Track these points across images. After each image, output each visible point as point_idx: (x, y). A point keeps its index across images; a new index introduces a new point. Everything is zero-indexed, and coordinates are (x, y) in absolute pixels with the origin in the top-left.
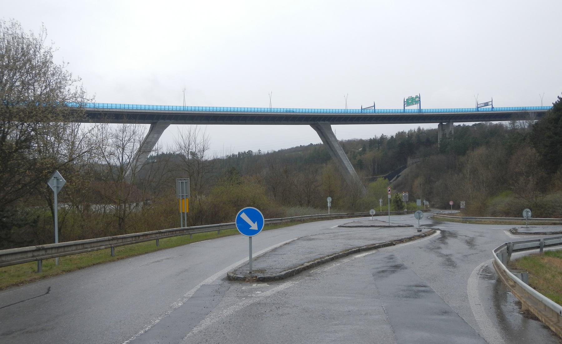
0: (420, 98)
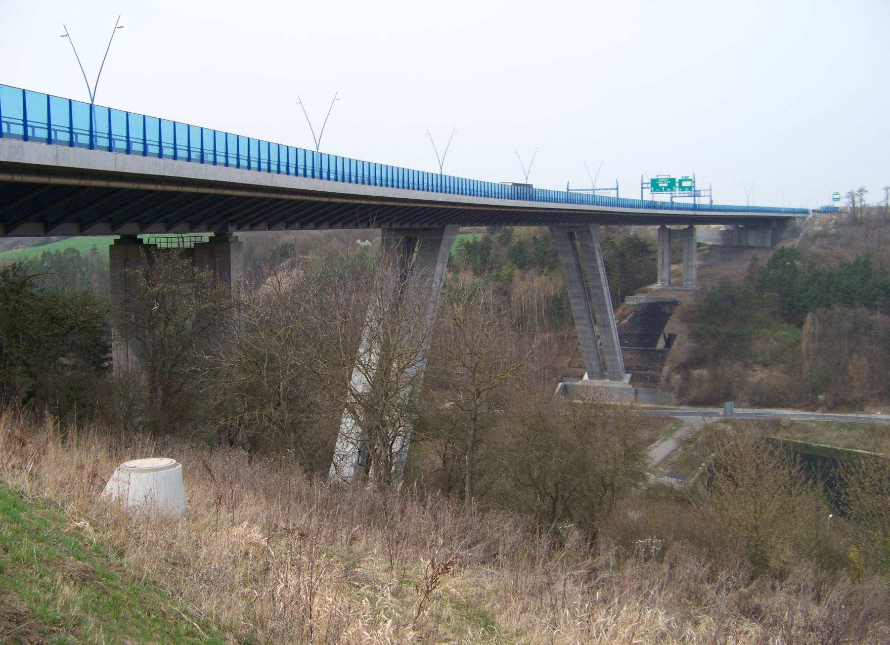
0: (694, 182)
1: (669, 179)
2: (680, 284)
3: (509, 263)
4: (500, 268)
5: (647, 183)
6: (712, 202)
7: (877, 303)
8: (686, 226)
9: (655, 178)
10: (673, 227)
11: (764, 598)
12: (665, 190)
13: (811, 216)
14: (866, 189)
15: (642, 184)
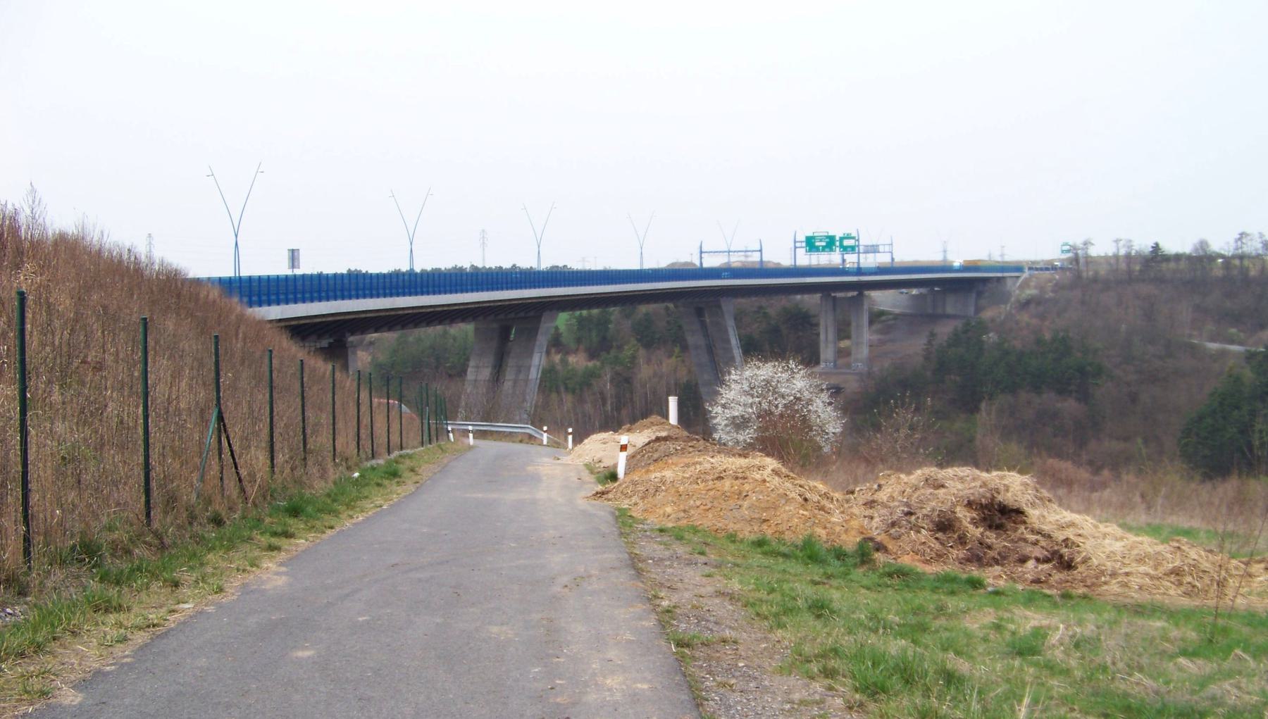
0: (858, 240)
1: (828, 237)
2: (848, 366)
3: (633, 341)
4: (620, 348)
5: (801, 242)
6: (893, 259)
7: (1073, 387)
8: (855, 293)
9: (811, 235)
10: (839, 295)
11: (473, 370)
12: (823, 250)
13: (1026, 274)
14: (1092, 242)
15: (795, 242)
